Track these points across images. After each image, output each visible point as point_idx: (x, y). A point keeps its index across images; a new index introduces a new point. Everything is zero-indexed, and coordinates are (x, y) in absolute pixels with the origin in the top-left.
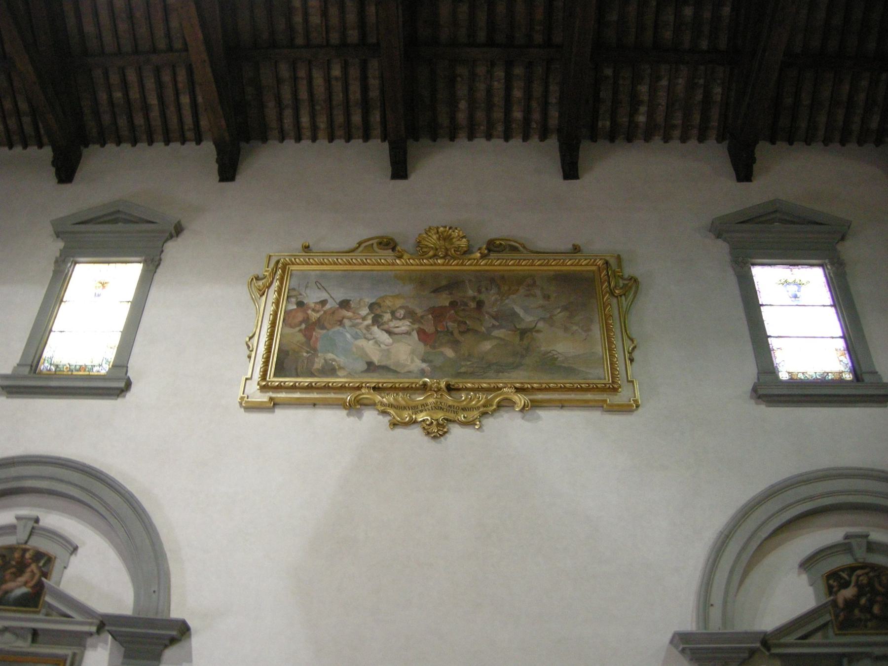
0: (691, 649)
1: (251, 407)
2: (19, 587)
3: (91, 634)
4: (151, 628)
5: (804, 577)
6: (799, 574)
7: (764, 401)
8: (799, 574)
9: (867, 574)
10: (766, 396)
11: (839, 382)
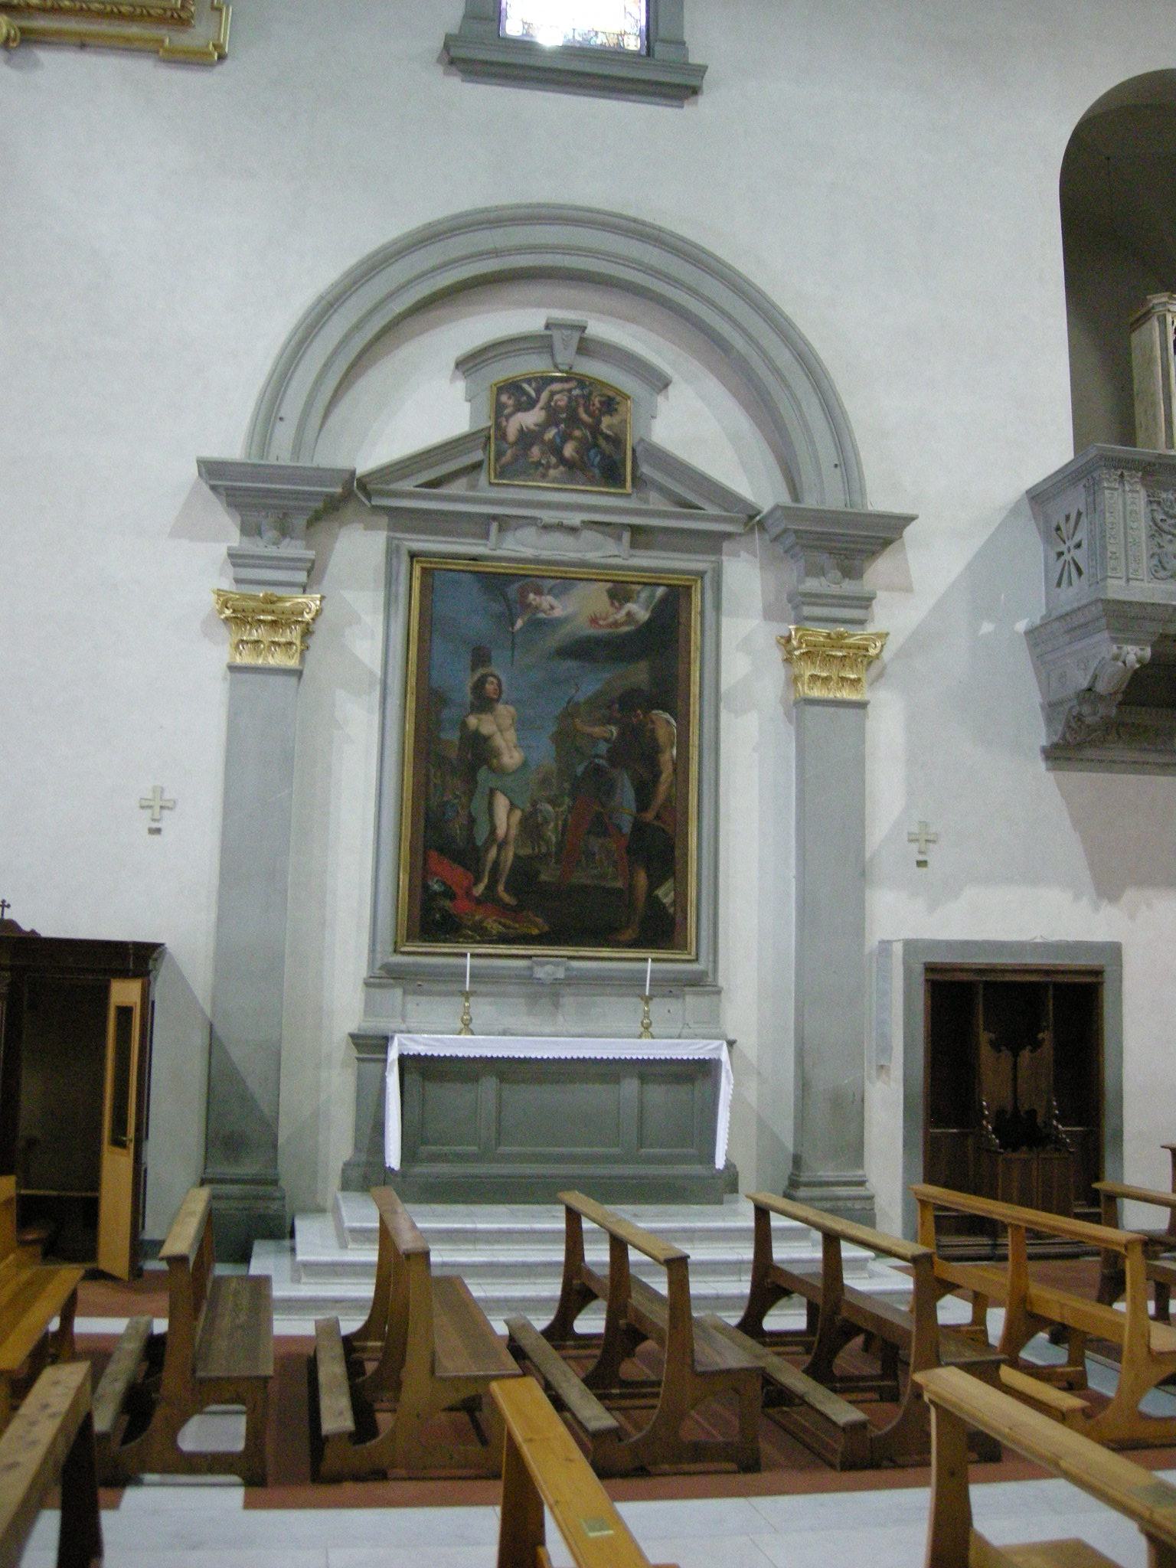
0: (227, 488)
3: (728, 536)
4: (556, 1146)
5: (461, 385)
6: (453, 379)
7: (461, 71)
8: (453, 379)
9: (570, 391)
10: (464, 61)
11: (615, 54)
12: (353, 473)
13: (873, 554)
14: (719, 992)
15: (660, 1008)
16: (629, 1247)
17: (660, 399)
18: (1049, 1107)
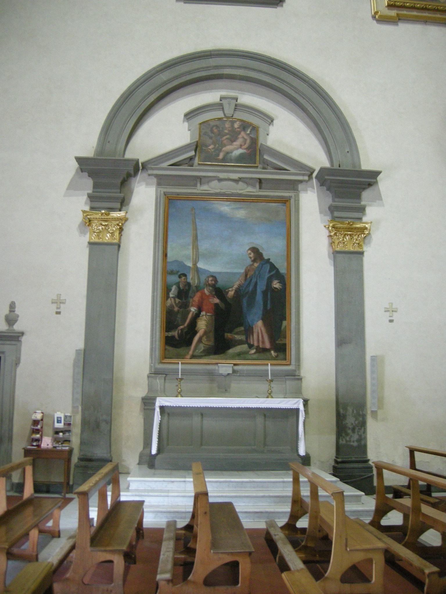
1: (382, 20)
2: (237, 149)
3: (301, 182)
5: (186, 124)
12: (137, 161)
16: (319, 489)
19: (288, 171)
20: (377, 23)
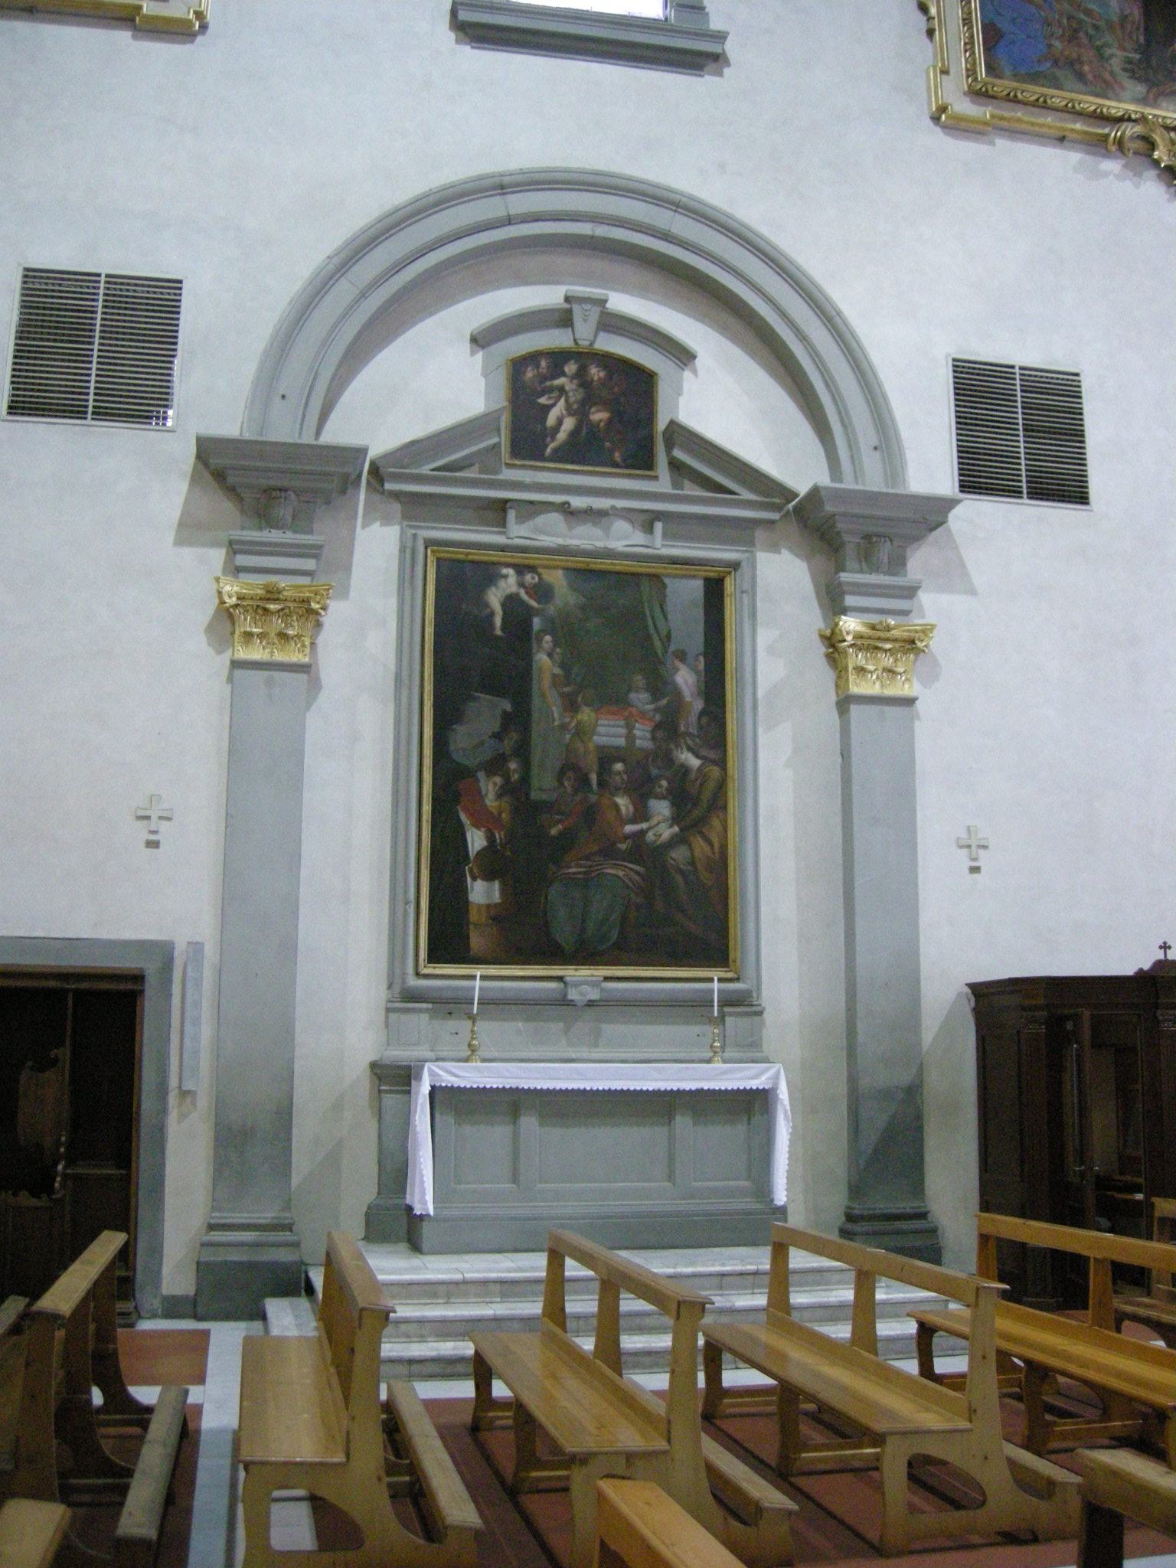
13: (916, 539)
14: (760, 1013)
15: (487, 1029)
17: (687, 374)
18: (58, 1144)
19: (733, 496)
20: (945, 134)
